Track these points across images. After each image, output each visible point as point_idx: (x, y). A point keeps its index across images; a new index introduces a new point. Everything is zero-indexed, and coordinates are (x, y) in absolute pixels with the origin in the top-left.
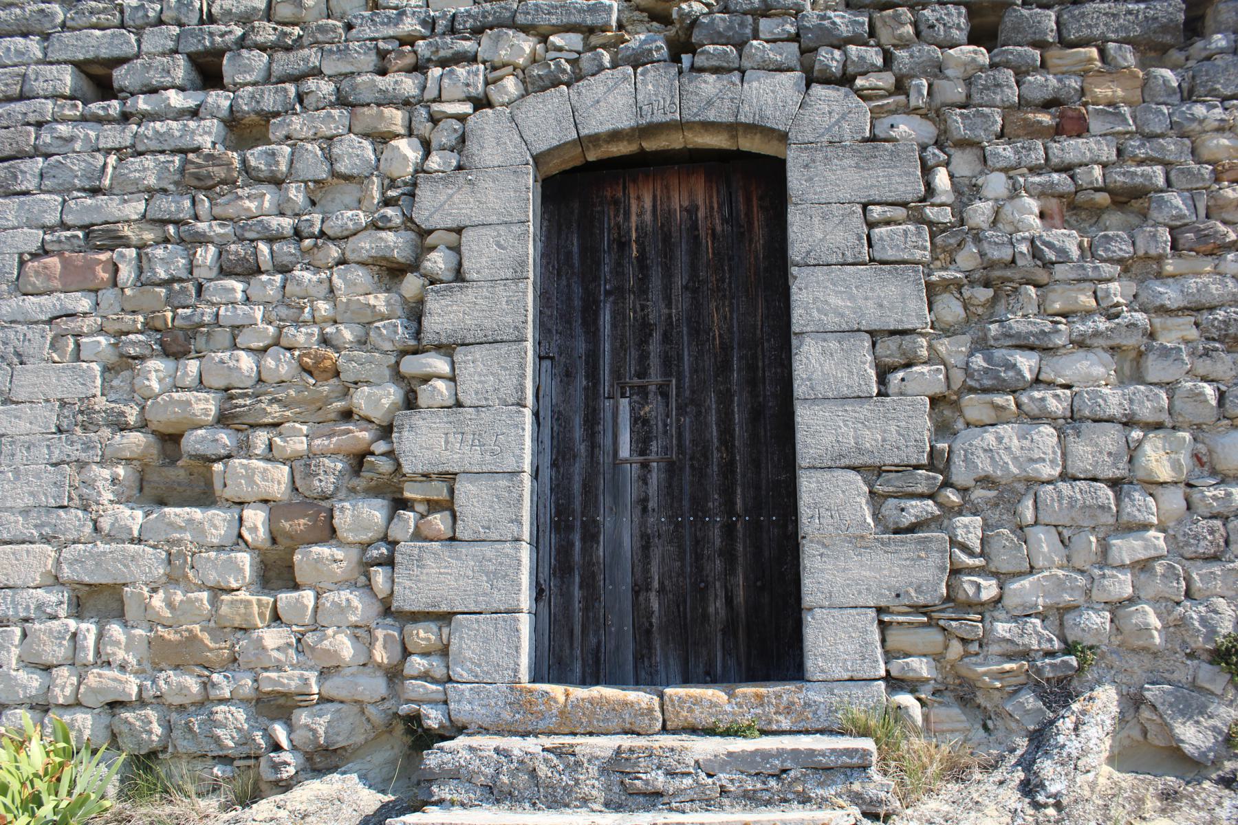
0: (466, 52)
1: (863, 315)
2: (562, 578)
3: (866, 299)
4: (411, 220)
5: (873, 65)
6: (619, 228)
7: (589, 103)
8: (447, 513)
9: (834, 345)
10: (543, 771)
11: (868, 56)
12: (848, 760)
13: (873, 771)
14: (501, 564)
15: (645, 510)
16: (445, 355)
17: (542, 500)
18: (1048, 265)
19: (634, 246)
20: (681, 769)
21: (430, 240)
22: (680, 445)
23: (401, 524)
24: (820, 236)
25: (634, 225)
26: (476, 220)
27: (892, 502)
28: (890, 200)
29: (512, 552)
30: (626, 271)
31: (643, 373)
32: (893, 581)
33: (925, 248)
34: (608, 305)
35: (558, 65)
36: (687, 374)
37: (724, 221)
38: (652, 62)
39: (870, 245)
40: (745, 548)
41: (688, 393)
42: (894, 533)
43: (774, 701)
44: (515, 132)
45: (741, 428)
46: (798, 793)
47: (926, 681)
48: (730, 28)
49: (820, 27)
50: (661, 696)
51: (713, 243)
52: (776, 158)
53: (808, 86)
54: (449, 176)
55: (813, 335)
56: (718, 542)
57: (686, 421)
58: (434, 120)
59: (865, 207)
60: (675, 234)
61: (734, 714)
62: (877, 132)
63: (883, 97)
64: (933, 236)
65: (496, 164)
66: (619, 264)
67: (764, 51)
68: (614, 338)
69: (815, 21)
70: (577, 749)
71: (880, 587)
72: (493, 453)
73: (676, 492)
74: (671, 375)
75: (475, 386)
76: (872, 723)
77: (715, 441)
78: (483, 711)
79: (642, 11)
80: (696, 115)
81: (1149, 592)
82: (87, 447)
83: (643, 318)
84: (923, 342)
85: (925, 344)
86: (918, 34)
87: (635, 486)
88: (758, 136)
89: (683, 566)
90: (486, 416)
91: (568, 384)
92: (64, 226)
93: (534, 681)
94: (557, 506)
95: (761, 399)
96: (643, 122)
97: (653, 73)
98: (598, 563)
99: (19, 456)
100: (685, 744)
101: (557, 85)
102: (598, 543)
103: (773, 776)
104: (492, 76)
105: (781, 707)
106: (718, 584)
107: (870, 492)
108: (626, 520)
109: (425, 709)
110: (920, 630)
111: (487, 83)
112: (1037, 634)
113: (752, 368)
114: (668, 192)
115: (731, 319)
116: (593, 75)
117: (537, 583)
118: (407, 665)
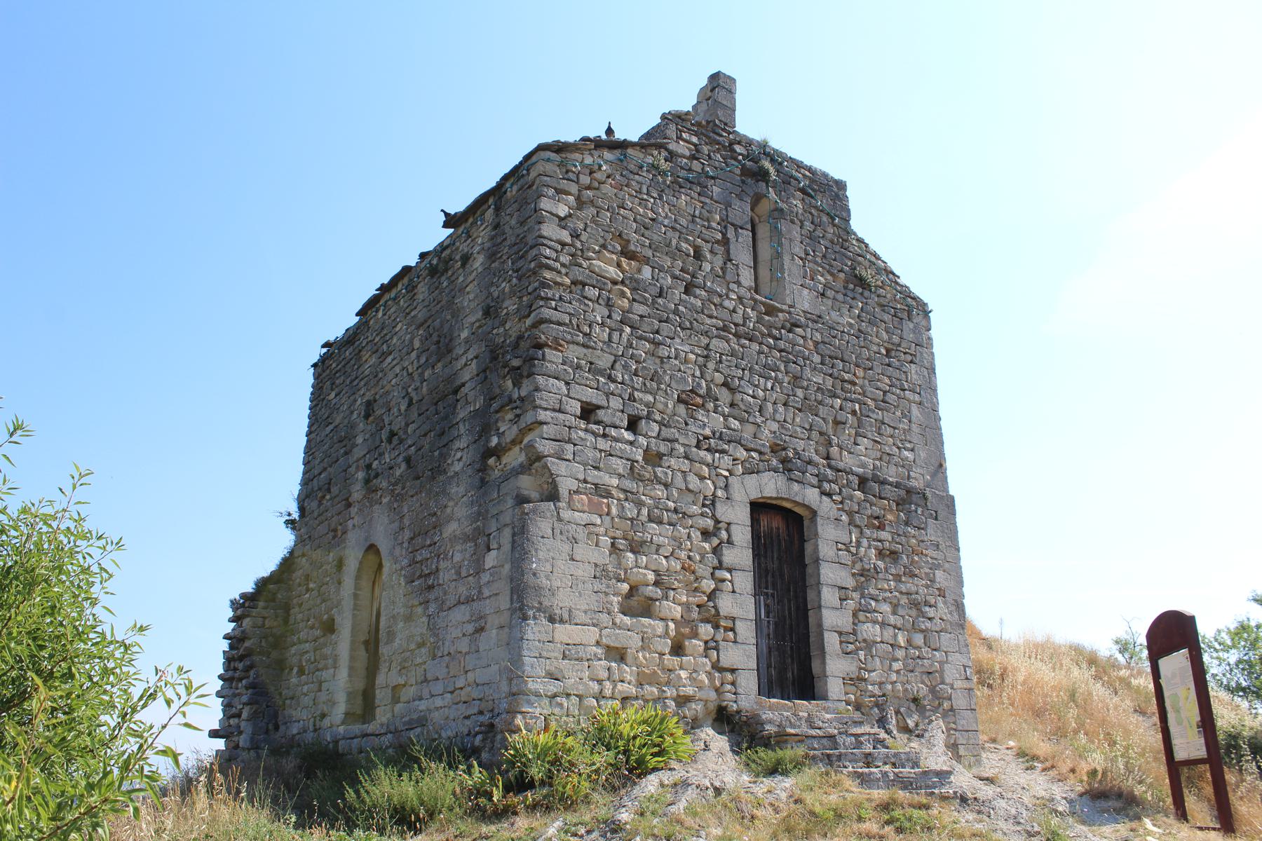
18: (878, 573)
21: (720, 525)
26: (736, 521)
81: (899, 680)
82: (608, 587)
92: (585, 481)
99: (580, 586)
112: (876, 690)
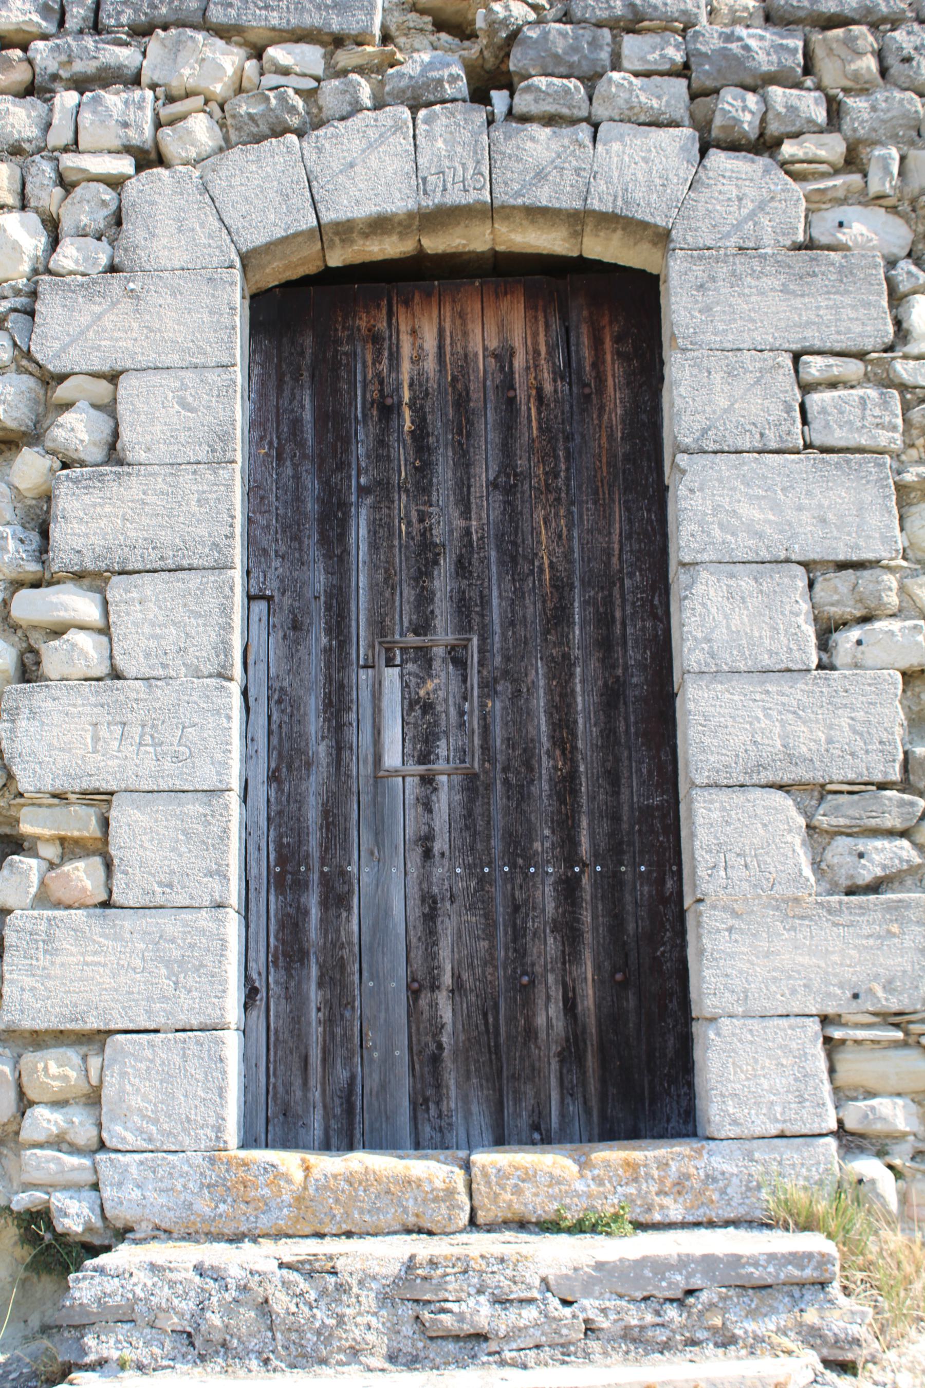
0: (120, 67)
1: (794, 535)
2: (288, 969)
3: (800, 509)
4: (28, 355)
5: (810, 121)
6: (381, 383)
7: (336, 166)
8: (97, 861)
9: (746, 584)
10: (281, 1303)
11: (802, 107)
12: (797, 1273)
13: (835, 1289)
14: (192, 946)
15: (427, 854)
16: (91, 589)
17: (254, 837)
19: (407, 413)
20: (518, 1292)
21: (62, 392)
22: (486, 748)
23: (15, 879)
24: (724, 403)
25: (405, 378)
26: (143, 360)
27: (842, 842)
28: (838, 347)
29: (212, 926)
30: (394, 455)
31: (422, 627)
32: (847, 973)
33: (894, 428)
34: (363, 512)
35: (282, 99)
36: (497, 628)
37: (558, 375)
38: (443, 102)
39: (805, 422)
40: (595, 917)
41: (498, 660)
42: (848, 894)
43: (656, 1173)
44: (210, 210)
45: (587, 719)
46: (714, 1330)
47: (900, 1137)
48: (575, 49)
49: (724, 54)
50: (467, 1166)
51: (539, 413)
52: (642, 273)
53: (703, 152)
54: (95, 282)
55: (712, 567)
56: (550, 907)
57: (497, 706)
58: (66, 184)
59: (796, 357)
60: (476, 395)
61: (589, 1196)
62: (815, 233)
63: (824, 175)
64: (906, 408)
65: (177, 265)
66: (381, 443)
67: (631, 91)
68: (374, 567)
69: (716, 43)
70: (340, 1264)
71: (828, 983)
72: (176, 757)
73: (480, 824)
74: (470, 630)
75: (144, 643)
76: (821, 1207)
77: (544, 739)
78: (163, 1200)
79: (422, 12)
80: (518, 194)
83: (423, 535)
84: (891, 580)
85: (895, 585)
86: (884, 72)
87: (411, 814)
88: (619, 233)
89: (492, 947)
90: (164, 694)
91: (297, 642)
93: (243, 1146)
94: (280, 846)
95: (620, 672)
96: (429, 203)
97: (444, 121)
98: (350, 943)
100: (524, 1249)
101: (282, 134)
102: (349, 909)
103: (672, 1301)
104: (167, 112)
105: (668, 1183)
106: (551, 978)
107: (808, 826)
108: (396, 871)
109: (58, 1200)
110: (892, 1053)
111: (158, 124)
113: (604, 620)
114: (464, 324)
115: (570, 538)
116: (343, 119)
117: (247, 978)
118: (27, 1122)
